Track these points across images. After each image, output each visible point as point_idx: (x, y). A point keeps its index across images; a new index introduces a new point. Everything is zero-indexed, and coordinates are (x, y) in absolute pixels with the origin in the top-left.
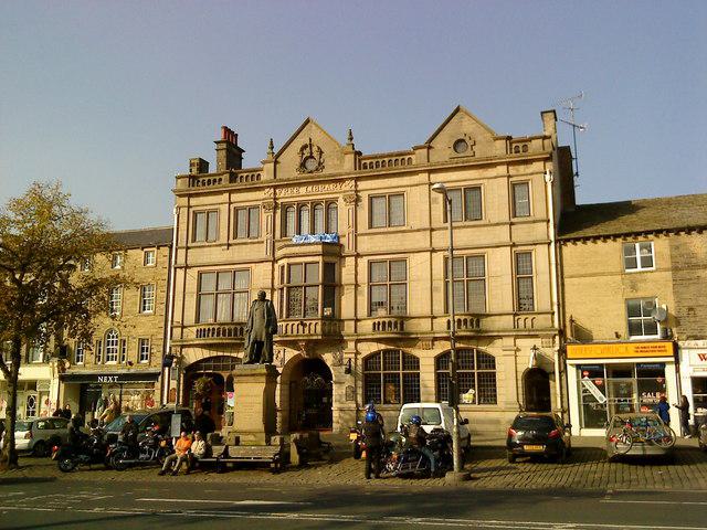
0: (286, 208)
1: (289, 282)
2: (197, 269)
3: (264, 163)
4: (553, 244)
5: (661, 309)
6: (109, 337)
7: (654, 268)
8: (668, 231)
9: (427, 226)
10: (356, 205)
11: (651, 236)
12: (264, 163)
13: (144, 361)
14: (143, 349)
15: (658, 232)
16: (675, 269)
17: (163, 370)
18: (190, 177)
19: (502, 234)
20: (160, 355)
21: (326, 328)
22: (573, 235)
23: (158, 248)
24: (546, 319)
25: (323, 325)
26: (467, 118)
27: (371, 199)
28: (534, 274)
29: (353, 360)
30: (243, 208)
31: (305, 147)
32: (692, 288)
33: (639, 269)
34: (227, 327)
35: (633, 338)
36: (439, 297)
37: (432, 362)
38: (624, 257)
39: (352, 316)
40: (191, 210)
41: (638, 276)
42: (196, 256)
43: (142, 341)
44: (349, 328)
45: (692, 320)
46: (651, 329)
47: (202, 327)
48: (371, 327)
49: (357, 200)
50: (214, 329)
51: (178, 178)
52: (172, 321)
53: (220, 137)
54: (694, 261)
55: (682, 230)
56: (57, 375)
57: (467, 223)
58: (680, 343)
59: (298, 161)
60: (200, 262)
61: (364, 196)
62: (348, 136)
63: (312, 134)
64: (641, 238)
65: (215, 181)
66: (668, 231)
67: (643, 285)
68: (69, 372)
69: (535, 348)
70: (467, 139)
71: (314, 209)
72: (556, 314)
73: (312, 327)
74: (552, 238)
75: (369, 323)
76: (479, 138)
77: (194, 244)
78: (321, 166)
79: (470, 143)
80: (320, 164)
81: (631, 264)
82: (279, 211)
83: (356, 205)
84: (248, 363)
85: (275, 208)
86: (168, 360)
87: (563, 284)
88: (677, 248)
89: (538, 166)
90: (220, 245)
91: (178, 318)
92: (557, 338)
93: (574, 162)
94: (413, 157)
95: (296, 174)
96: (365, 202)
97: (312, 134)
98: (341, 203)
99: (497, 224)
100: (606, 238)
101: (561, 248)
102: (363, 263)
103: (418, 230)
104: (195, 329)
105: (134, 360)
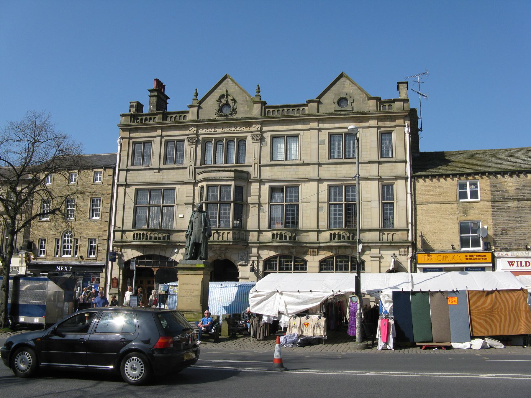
0: (206, 142)
1: (207, 199)
2: (133, 188)
3: (190, 107)
4: (409, 180)
5: (483, 228)
6: (65, 236)
7: (479, 199)
8: (490, 173)
9: (315, 160)
10: (261, 143)
11: (477, 177)
12: (190, 107)
13: (93, 256)
14: (91, 247)
15: (483, 174)
16: (494, 201)
17: (107, 263)
18: (131, 115)
19: (372, 170)
20: (105, 251)
21: (236, 237)
22: (424, 173)
23: (105, 170)
24: (402, 234)
25: (234, 234)
26: (348, 81)
27: (273, 138)
28: (395, 201)
29: (256, 262)
30: (140, 143)
31: (222, 96)
32: (505, 214)
33: (469, 199)
34: (145, 233)
35: (464, 249)
36: (324, 216)
37: (317, 264)
38: (458, 191)
39: (256, 228)
40: (131, 141)
41: (468, 204)
42: (135, 177)
43: (91, 241)
44: (253, 237)
45: (505, 237)
46: (476, 243)
47: (333, 232)
48: (328, 237)
49: (262, 140)
50: (140, 234)
51: (123, 116)
52: (115, 226)
53: (153, 86)
54: (506, 195)
55: (498, 173)
56: (24, 264)
57: (331, 161)
58: (496, 254)
59: (217, 106)
60: (136, 181)
61: (268, 137)
62: (194, 93)
63: (228, 86)
64: (470, 178)
65: (146, 119)
66: (490, 173)
67: (471, 211)
68: (33, 262)
69: (394, 256)
70: (348, 97)
71: (227, 144)
72: (410, 232)
73: (225, 235)
74: (409, 174)
75: (270, 234)
76: (356, 97)
77: (132, 167)
78: (234, 111)
79: (350, 101)
80: (234, 110)
81: (463, 195)
82: (200, 146)
83: (261, 143)
84: (189, 259)
85: (197, 142)
86: (112, 256)
87: (415, 209)
88: (495, 185)
89: (399, 122)
90: (153, 169)
91: (119, 224)
92: (410, 249)
93: (419, 121)
94: (306, 108)
95: (161, 121)
96: (268, 140)
97: (228, 86)
98: (249, 140)
99: (369, 163)
100: (447, 176)
101: (414, 182)
102: (265, 188)
103: (309, 164)
104: (328, 233)
105: (85, 255)
